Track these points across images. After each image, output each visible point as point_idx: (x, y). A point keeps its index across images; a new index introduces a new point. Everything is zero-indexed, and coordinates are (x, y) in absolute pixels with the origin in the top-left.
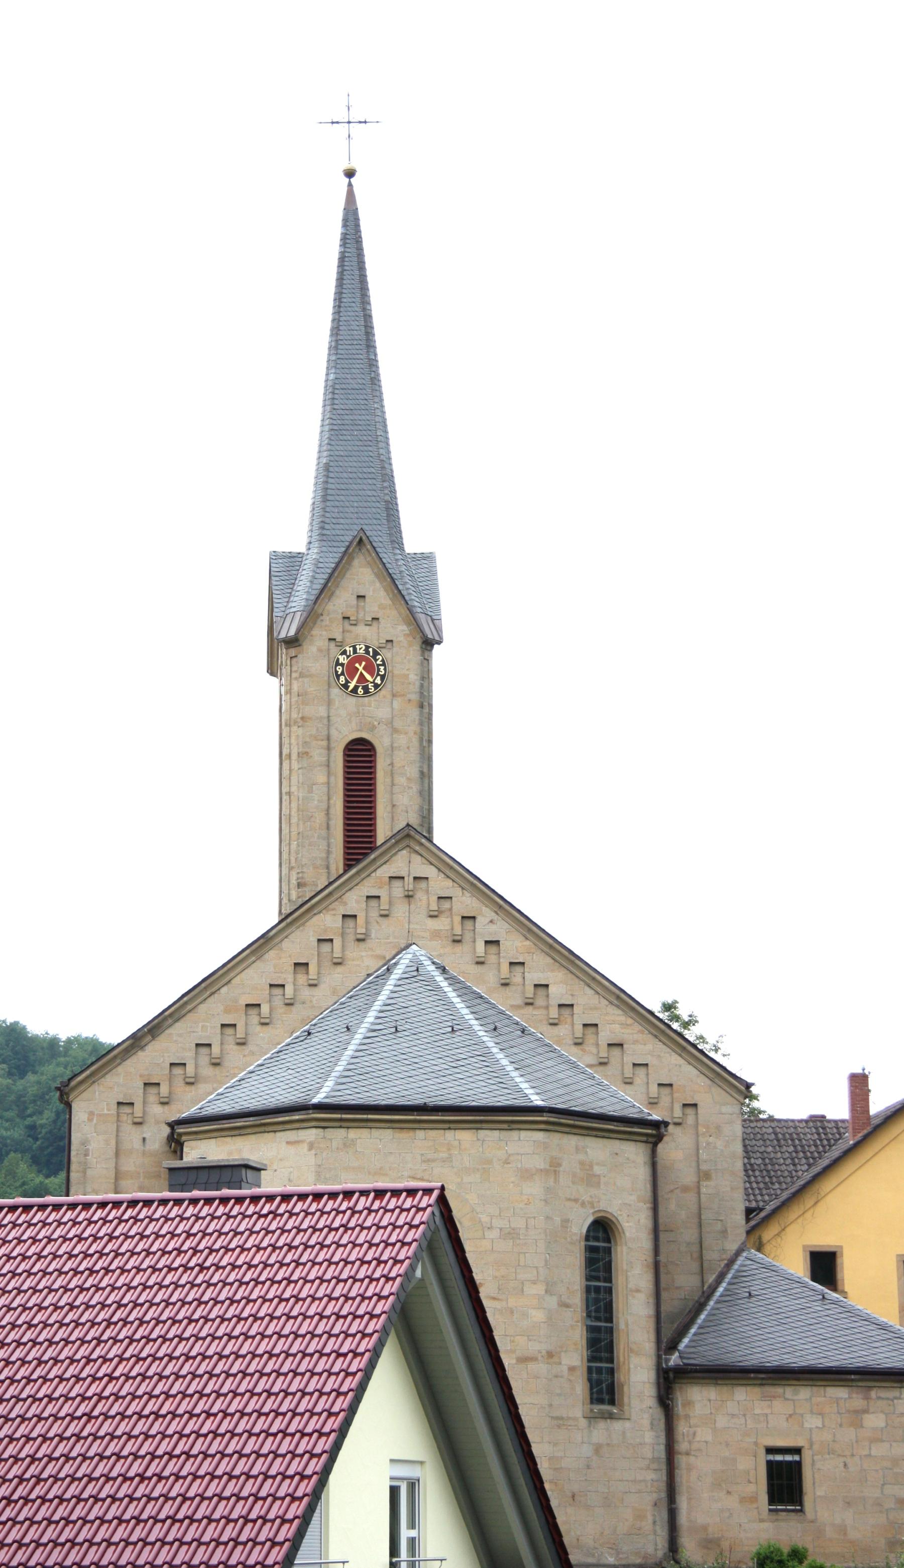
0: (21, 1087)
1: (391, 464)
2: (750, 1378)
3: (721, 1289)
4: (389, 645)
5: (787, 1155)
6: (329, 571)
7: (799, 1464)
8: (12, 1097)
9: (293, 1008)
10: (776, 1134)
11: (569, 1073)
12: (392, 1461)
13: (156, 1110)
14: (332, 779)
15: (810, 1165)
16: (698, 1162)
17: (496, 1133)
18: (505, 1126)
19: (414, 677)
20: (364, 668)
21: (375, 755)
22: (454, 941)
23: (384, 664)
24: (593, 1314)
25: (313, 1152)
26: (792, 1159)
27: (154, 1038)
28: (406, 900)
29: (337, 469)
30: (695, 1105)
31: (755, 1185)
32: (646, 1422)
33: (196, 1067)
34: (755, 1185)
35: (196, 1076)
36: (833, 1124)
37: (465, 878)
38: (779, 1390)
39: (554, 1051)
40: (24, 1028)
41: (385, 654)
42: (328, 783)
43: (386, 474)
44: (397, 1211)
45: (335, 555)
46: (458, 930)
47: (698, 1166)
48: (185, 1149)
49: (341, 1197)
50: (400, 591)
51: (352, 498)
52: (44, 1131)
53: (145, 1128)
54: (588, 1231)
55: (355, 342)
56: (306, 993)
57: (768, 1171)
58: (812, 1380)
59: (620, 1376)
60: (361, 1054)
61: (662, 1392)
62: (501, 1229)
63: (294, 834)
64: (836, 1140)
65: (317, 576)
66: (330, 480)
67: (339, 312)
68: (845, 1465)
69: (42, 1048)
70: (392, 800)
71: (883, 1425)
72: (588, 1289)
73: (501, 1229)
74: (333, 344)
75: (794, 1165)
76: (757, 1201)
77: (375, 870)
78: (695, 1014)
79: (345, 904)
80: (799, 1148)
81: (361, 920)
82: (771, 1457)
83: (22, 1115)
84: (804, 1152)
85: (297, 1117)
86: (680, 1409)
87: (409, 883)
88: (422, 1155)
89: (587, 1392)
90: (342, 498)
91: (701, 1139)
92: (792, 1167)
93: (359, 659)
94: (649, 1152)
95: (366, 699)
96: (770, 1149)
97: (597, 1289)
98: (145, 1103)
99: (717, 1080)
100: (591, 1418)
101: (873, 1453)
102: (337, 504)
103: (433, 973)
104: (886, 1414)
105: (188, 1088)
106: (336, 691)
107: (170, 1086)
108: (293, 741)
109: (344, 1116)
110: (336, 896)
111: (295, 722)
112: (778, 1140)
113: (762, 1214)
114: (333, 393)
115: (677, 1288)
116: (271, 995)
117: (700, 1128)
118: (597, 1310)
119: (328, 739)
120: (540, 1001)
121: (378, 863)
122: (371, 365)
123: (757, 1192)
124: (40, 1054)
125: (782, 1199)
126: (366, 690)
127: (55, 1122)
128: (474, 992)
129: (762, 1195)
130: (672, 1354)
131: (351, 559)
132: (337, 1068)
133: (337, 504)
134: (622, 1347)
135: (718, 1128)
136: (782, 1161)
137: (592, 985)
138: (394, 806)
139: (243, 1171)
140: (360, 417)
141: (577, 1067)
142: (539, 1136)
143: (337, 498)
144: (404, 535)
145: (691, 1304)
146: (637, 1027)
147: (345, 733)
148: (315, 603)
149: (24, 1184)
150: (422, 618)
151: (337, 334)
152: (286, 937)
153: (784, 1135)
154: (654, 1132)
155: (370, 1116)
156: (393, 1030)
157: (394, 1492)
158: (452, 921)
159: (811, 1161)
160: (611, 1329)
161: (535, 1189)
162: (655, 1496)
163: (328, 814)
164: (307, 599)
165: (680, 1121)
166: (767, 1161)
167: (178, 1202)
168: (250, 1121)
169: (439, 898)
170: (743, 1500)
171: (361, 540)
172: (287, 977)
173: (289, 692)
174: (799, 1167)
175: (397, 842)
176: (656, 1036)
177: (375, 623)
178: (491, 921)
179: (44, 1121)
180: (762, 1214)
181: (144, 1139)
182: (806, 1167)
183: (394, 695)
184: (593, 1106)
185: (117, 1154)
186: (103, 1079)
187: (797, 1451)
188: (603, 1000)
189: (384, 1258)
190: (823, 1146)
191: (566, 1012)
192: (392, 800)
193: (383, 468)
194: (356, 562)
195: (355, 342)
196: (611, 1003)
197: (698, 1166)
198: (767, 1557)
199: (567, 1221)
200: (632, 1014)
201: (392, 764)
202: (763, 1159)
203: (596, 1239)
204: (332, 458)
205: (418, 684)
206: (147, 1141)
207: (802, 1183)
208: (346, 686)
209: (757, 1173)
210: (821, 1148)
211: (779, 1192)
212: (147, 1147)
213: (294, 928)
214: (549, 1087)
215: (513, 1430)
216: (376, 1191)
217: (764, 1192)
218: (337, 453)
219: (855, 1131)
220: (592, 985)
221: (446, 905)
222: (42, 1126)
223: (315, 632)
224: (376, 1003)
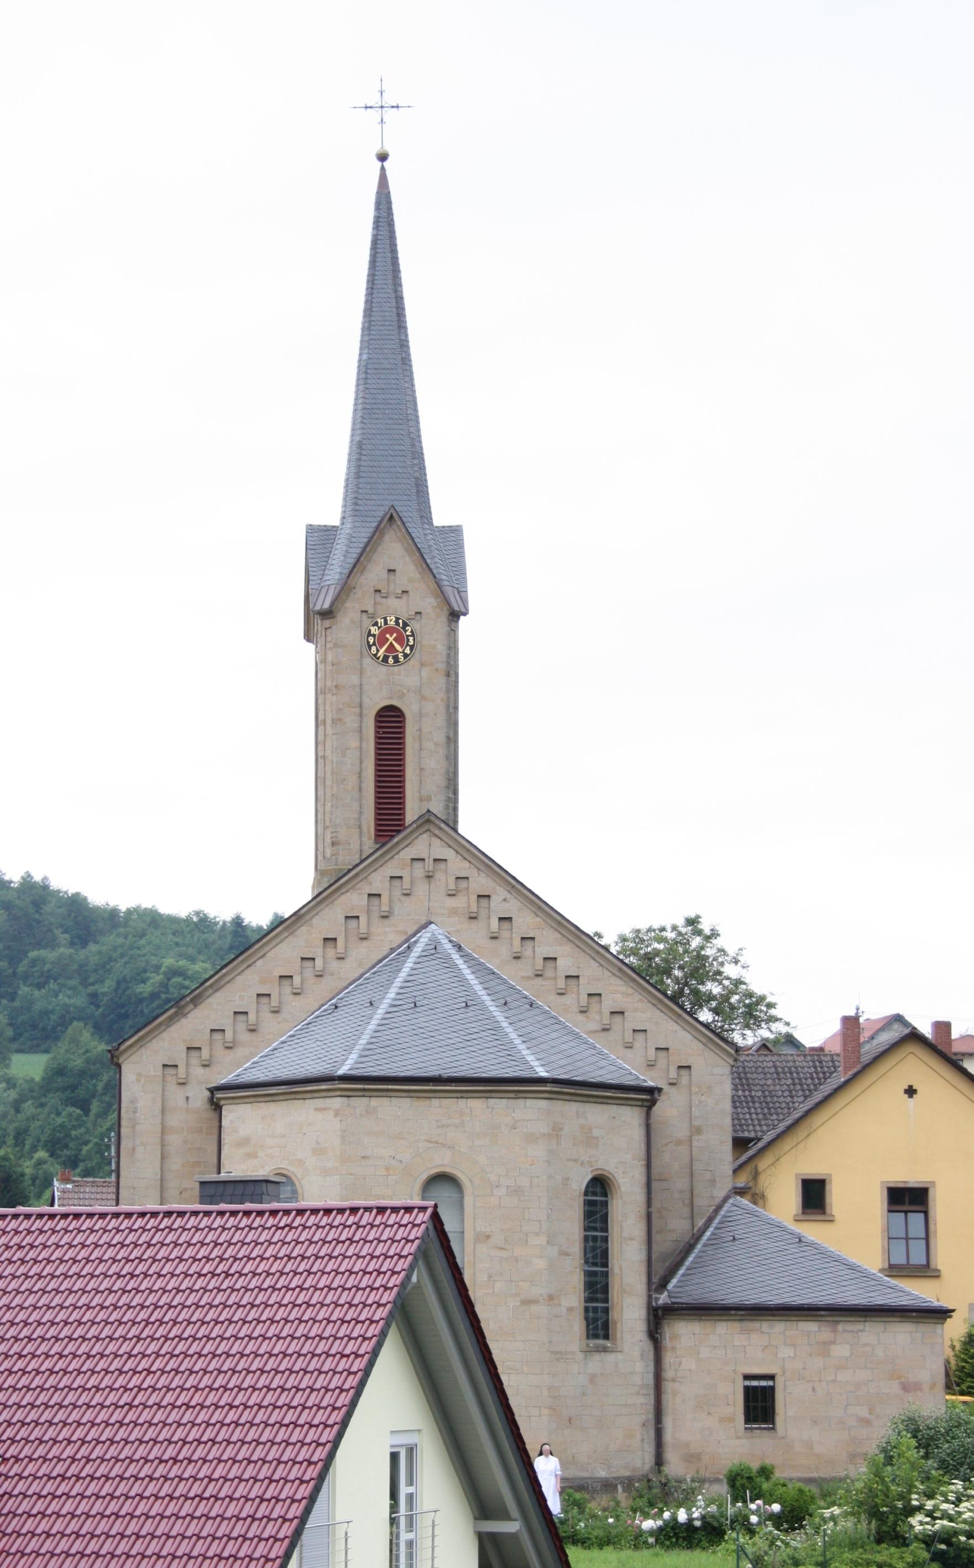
0: (83, 957)
1: (420, 442)
2: (731, 1315)
3: (708, 1234)
4: (418, 617)
5: (785, 1087)
6: (362, 545)
7: (772, 1389)
8: (75, 966)
9: (323, 979)
10: (776, 1067)
11: (573, 1044)
12: (392, 1432)
13: (198, 1071)
14: (364, 744)
15: (806, 1097)
16: (691, 1118)
18: (512, 1095)
19: (441, 648)
20: (395, 639)
21: (403, 721)
22: (471, 918)
23: (413, 635)
24: (591, 1260)
25: (338, 1118)
26: (790, 1091)
27: (195, 1006)
28: (427, 880)
29: (369, 447)
30: (689, 1067)
31: (754, 1116)
32: (636, 1353)
33: (235, 1032)
34: (754, 1116)
35: (234, 1041)
36: (829, 1058)
37: (480, 860)
38: (756, 1325)
39: (559, 1023)
40: (85, 899)
41: (415, 625)
42: (361, 748)
43: (416, 452)
44: (396, 1226)
45: (368, 530)
47: (691, 1121)
48: (224, 1113)
49: (348, 1212)
50: (427, 565)
51: (383, 475)
52: (105, 999)
53: (188, 1087)
54: (587, 1187)
55: (387, 323)
56: (334, 965)
57: (767, 1103)
58: (786, 1315)
59: (613, 1315)
60: (383, 1028)
61: (652, 1327)
62: (508, 1187)
63: (329, 795)
64: (831, 1073)
65: (350, 550)
66: (363, 458)
67: (372, 294)
68: (814, 1389)
69: (103, 919)
70: (420, 764)
71: (847, 1354)
72: (586, 1239)
73: (508, 1187)
74: (366, 325)
75: (792, 1097)
76: (755, 1131)
77: (398, 853)
78: (717, 928)
79: (370, 883)
80: (797, 1081)
81: (385, 899)
82: (748, 1383)
83: (84, 982)
84: (801, 1085)
85: (324, 1087)
86: (667, 1342)
87: (429, 864)
88: (437, 1121)
89: (584, 1329)
90: (374, 475)
91: (693, 1097)
92: (789, 1099)
93: (391, 630)
94: (644, 1115)
95: (396, 668)
96: (770, 1082)
97: (595, 1239)
99: (709, 1045)
100: (588, 1352)
101: (839, 1378)
102: (369, 480)
103: (449, 951)
104: (851, 1345)
105: (227, 1051)
106: (368, 661)
107: (211, 1049)
108: (328, 708)
109: (366, 1087)
110: (361, 877)
111: (330, 690)
112: (778, 1074)
113: (760, 1145)
114: (366, 373)
115: (669, 1231)
116: (302, 967)
117: (693, 1088)
118: (594, 1257)
119: (361, 706)
120: (549, 973)
121: (401, 846)
122: (402, 346)
123: (756, 1122)
124: (101, 925)
125: (779, 1130)
126: (396, 659)
127: (116, 990)
128: (488, 969)
129: (760, 1125)
130: (662, 1294)
131: (382, 534)
132: (361, 1042)
133: (369, 480)
134: (616, 1287)
135: (709, 1088)
136: (780, 1093)
137: (597, 958)
138: (422, 769)
139: (264, 1185)
140: (391, 397)
141: (579, 1037)
142: (543, 1104)
143: (370, 475)
144: (433, 510)
145: (681, 1245)
146: (637, 996)
148: (348, 577)
149: (87, 1051)
150: (449, 591)
151: (370, 316)
152: (316, 914)
153: (783, 1068)
154: (648, 1097)
155: (390, 1087)
156: (413, 1005)
157: (394, 1457)
158: (469, 899)
159: (807, 1093)
160: (607, 1272)
161: (538, 1151)
162: (644, 1417)
163: (360, 777)
164: (341, 573)
165: (675, 1081)
166: (767, 1093)
167: (207, 1214)
168: (283, 1089)
169: (457, 878)
170: (722, 1420)
171: (391, 517)
172: (317, 952)
173: (324, 661)
174: (796, 1099)
175: (418, 827)
176: (654, 1005)
177: (405, 596)
179: (105, 990)
180: (760, 1145)
181: (187, 1098)
182: (802, 1099)
183: (422, 665)
184: (593, 1075)
185: (163, 1111)
186: (150, 1044)
187: (772, 1377)
188: (606, 971)
189: (383, 1269)
190: (819, 1079)
191: (573, 982)
192: (420, 764)
193: (413, 445)
194: (387, 538)
195: (387, 323)
196: (614, 975)
197: (691, 1121)
198: (738, 1475)
199: (568, 1179)
200: (631, 984)
201: (420, 730)
202: (763, 1092)
203: (595, 1194)
204: (365, 436)
205: (444, 654)
206: (190, 1100)
207: (798, 1115)
209: (757, 1105)
210: (817, 1081)
211: (776, 1122)
212: (190, 1105)
213: (322, 906)
214: (554, 1058)
215: (498, 1402)
216: (377, 1208)
217: (763, 1122)
218: (370, 431)
219: (846, 1069)
220: (597, 958)
221: (463, 884)
222: (104, 994)
223: (348, 604)
224: (397, 980)
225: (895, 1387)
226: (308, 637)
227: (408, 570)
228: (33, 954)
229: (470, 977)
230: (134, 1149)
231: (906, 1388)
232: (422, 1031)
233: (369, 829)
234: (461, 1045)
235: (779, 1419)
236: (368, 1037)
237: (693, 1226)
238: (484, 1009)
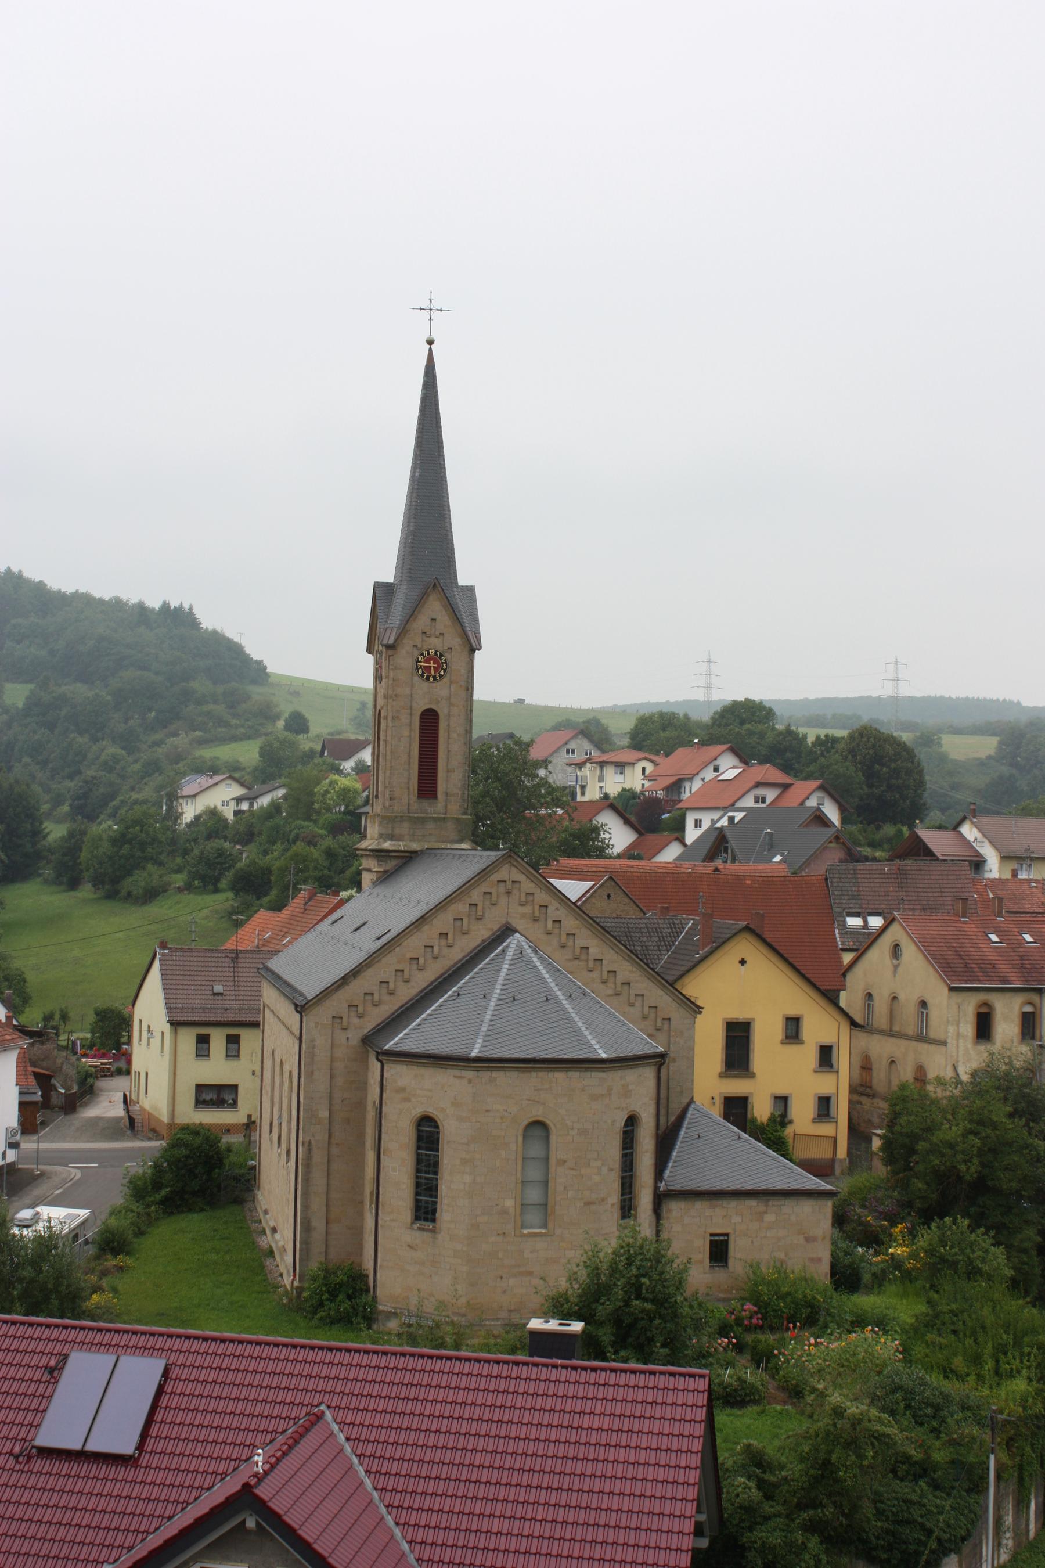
7: (727, 1242)
17: (578, 1074)
23: (446, 662)
26: (658, 946)
33: (380, 994)
38: (719, 1202)
42: (410, 736)
46: (537, 914)
56: (446, 951)
68: (752, 1242)
71: (773, 1219)
75: (660, 950)
79: (471, 897)
81: (479, 907)
82: (712, 1238)
86: (664, 1214)
87: (509, 885)
93: (431, 658)
98: (349, 1016)
101: (769, 1234)
106: (416, 679)
112: (649, 933)
119: (411, 708)
138: (449, 751)
147: (421, 705)
150: (470, 634)
156: (512, 999)
177: (441, 637)
178: (557, 909)
181: (348, 1038)
183: (451, 682)
187: (727, 1235)
194: (431, 598)
196: (625, 959)
201: (449, 725)
208: (422, 676)
221: (530, 898)
223: (405, 641)
225: (801, 1240)
226: (370, 650)
227: (444, 619)
228: (13, 621)
229: (547, 976)
230: (312, 1073)
231: (808, 1240)
232: (521, 1020)
233: (414, 790)
234: (547, 1031)
235: (731, 1262)
236: (486, 1025)
237: (668, 1122)
238: (559, 1002)
